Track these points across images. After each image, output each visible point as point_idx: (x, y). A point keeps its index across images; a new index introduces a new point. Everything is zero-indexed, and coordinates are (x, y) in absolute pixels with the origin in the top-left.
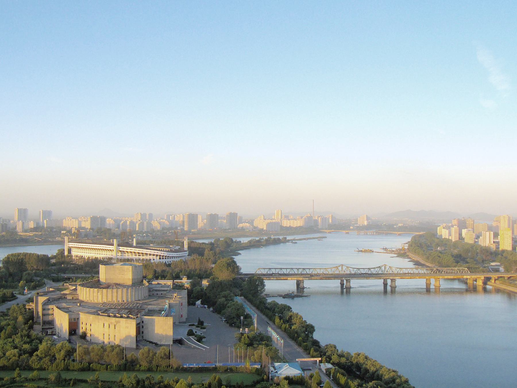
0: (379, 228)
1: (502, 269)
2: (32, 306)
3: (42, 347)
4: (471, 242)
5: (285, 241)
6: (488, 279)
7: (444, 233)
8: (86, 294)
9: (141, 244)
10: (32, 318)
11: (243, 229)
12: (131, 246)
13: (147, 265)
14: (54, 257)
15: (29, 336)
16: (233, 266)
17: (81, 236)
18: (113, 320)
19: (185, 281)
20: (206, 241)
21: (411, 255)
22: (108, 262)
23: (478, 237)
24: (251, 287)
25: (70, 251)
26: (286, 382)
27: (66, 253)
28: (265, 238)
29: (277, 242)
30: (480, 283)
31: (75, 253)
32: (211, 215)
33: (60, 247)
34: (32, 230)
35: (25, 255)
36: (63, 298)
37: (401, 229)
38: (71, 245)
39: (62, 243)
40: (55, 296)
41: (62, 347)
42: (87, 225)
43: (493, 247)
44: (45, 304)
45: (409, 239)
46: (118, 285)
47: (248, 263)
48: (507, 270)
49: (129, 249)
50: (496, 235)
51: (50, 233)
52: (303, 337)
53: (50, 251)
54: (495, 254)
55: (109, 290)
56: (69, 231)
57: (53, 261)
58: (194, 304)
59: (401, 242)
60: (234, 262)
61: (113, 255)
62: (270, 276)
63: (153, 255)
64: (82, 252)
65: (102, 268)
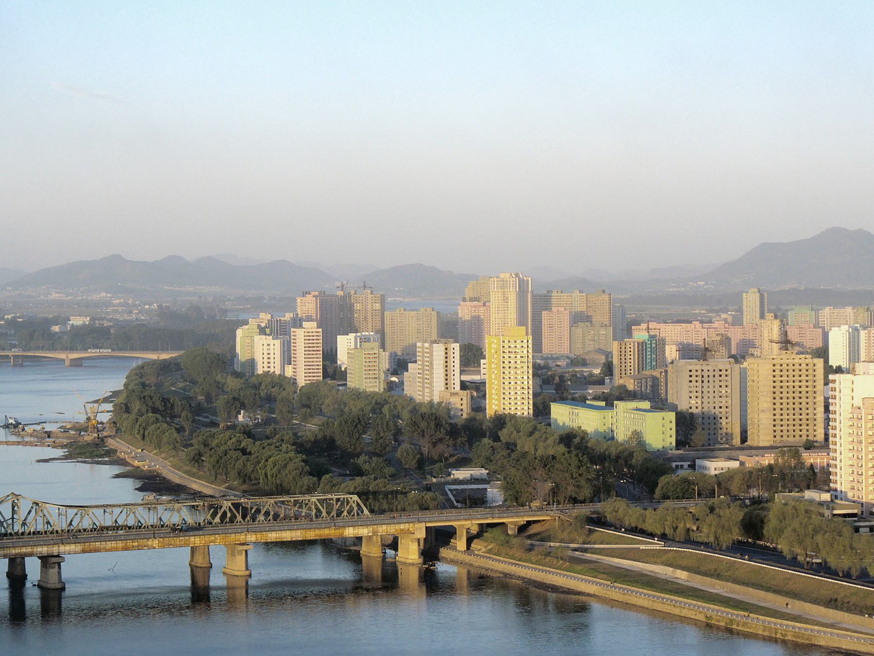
7: (260, 351)
23: (400, 365)
30: (410, 554)
37: (93, 336)
43: (461, 404)
45: (117, 382)
50: (472, 356)
59: (83, 395)
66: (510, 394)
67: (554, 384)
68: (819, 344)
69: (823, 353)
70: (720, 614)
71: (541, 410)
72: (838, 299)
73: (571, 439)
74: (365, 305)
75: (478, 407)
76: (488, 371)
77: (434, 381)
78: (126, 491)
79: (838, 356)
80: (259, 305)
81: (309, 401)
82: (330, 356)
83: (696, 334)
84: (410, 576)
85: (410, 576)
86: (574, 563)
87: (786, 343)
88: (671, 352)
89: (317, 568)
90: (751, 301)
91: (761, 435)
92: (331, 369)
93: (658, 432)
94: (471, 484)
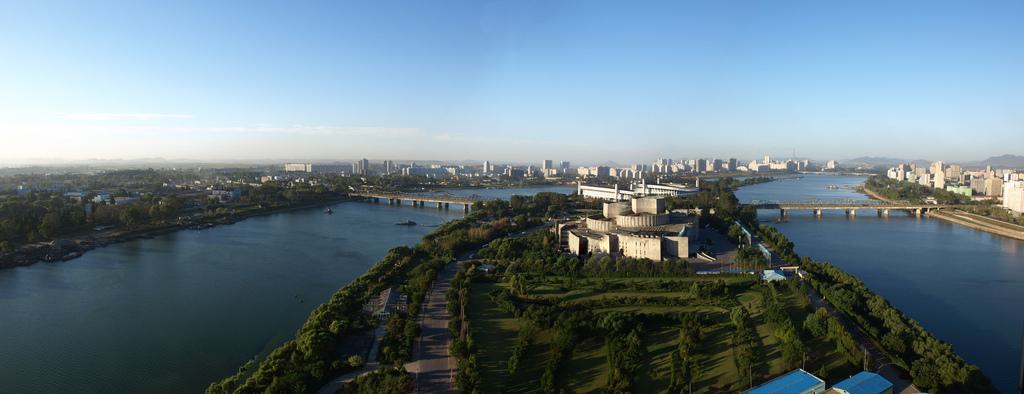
0: (842, 171)
1: (935, 203)
2: (554, 230)
3: (559, 260)
4: (913, 182)
5: (772, 180)
6: (925, 210)
7: (891, 174)
8: (592, 224)
9: (664, 182)
10: (553, 238)
11: (740, 171)
12: (629, 190)
13: (668, 198)
14: (570, 196)
15: (550, 251)
16: (733, 200)
17: (591, 181)
18: (643, 240)
19: (698, 211)
20: (713, 180)
21: (866, 190)
22: (610, 202)
23: (918, 178)
24: (748, 217)
25: (582, 192)
26: (773, 284)
27: (579, 193)
28: (757, 177)
29: (766, 180)
30: (918, 212)
31: (585, 193)
32: (731, 160)
33: (574, 189)
34: (555, 176)
35: (550, 193)
36: (575, 226)
37: (862, 171)
38: (583, 187)
39: (576, 186)
40: (569, 224)
41: (605, 261)
42: (595, 173)
43: (929, 185)
44: (562, 229)
45: (866, 179)
46: (646, 213)
47: (746, 196)
48: (939, 203)
49: (654, 187)
50: (932, 176)
51: (568, 176)
52: (785, 253)
53: (567, 191)
54: (927, 191)
55: (640, 218)
56: (582, 177)
57: (570, 199)
58: (704, 227)
59: (860, 182)
60: (734, 196)
61: (614, 196)
62: (760, 207)
63: (672, 190)
64: (591, 192)
65: (605, 206)
66: (939, 183)
67: (948, 183)
68: (989, 236)
69: (1003, 178)
70: (978, 227)
71: (945, 187)
72: (1007, 168)
73: (952, 193)
74: (912, 167)
75: (933, 186)
76: (935, 180)
77: (924, 181)
78: (866, 198)
79: (1006, 179)
80: (892, 166)
81: (901, 183)
82: (905, 175)
83: (977, 174)
84: (918, 216)
85: (918, 216)
86: (950, 216)
87: (995, 176)
88: (971, 177)
89: (901, 214)
90: (989, 168)
91: (989, 194)
92: (905, 179)
93: (968, 192)
94: (658, 316)
